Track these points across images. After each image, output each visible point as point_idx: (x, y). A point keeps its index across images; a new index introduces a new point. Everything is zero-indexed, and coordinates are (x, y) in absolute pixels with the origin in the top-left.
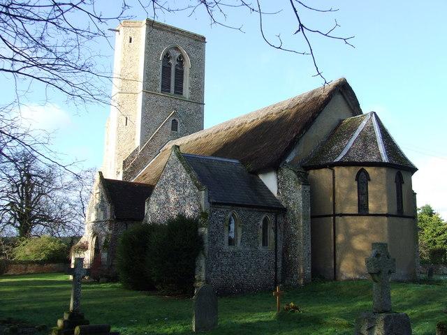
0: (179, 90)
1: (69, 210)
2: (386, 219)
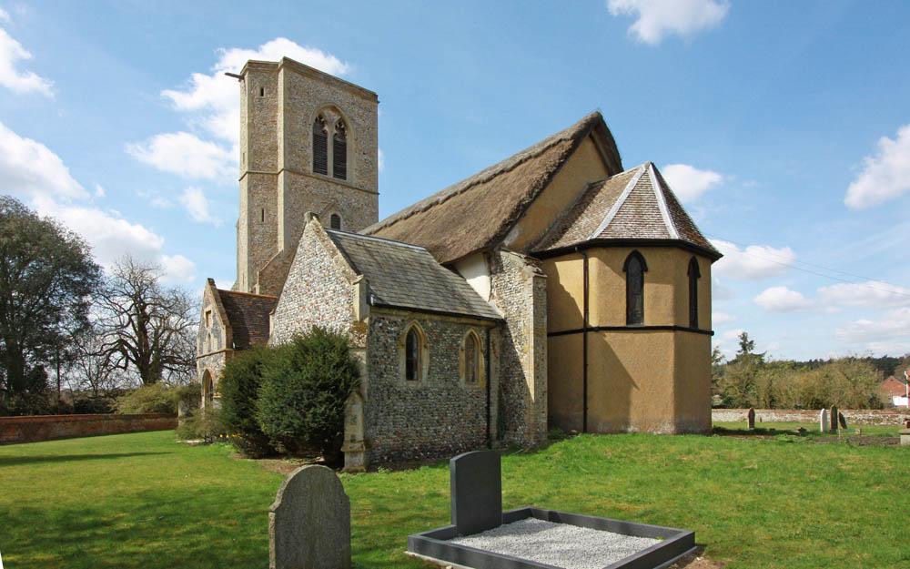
0: (340, 171)
1: (747, 368)
2: (670, 335)
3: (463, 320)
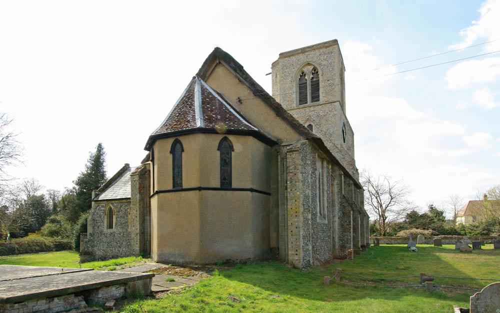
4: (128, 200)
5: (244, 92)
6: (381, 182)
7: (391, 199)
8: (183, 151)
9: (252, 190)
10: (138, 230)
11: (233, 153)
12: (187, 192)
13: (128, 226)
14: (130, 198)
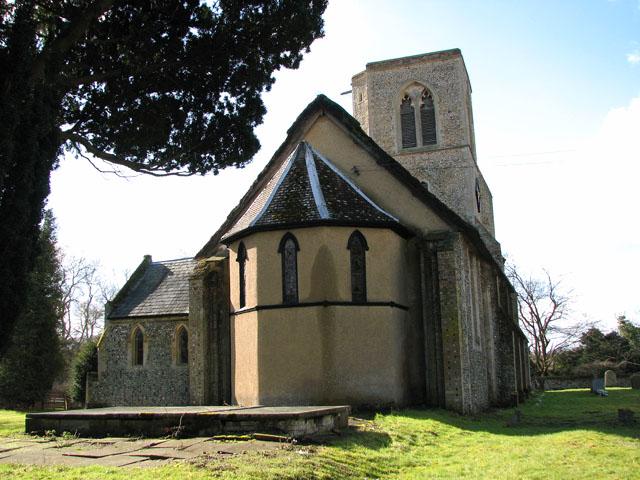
3: (172, 318)
4: (184, 318)
5: (362, 159)
6: (535, 278)
7: (555, 308)
8: (297, 248)
9: (392, 304)
10: (202, 365)
11: (367, 252)
12: (306, 308)
13: (170, 359)
14: (187, 315)
